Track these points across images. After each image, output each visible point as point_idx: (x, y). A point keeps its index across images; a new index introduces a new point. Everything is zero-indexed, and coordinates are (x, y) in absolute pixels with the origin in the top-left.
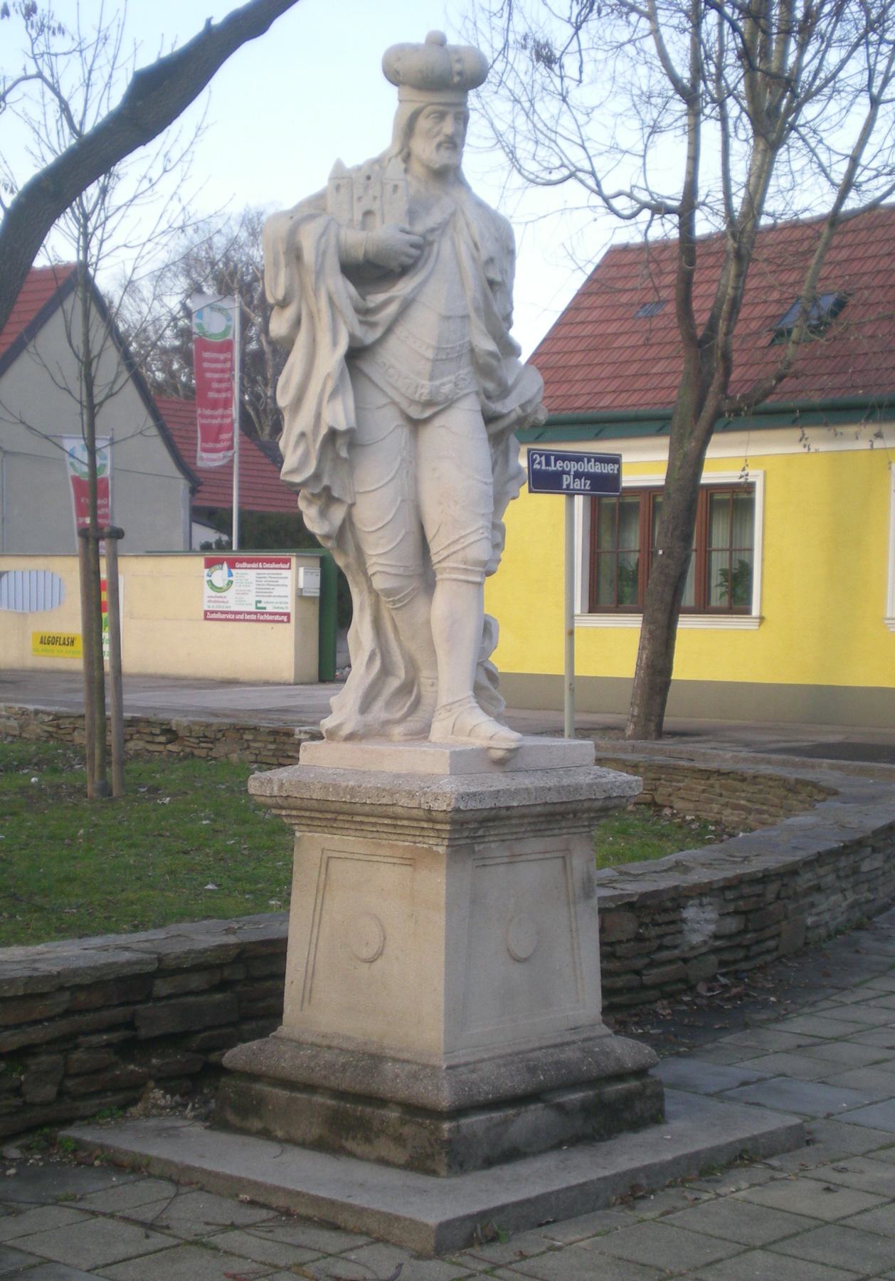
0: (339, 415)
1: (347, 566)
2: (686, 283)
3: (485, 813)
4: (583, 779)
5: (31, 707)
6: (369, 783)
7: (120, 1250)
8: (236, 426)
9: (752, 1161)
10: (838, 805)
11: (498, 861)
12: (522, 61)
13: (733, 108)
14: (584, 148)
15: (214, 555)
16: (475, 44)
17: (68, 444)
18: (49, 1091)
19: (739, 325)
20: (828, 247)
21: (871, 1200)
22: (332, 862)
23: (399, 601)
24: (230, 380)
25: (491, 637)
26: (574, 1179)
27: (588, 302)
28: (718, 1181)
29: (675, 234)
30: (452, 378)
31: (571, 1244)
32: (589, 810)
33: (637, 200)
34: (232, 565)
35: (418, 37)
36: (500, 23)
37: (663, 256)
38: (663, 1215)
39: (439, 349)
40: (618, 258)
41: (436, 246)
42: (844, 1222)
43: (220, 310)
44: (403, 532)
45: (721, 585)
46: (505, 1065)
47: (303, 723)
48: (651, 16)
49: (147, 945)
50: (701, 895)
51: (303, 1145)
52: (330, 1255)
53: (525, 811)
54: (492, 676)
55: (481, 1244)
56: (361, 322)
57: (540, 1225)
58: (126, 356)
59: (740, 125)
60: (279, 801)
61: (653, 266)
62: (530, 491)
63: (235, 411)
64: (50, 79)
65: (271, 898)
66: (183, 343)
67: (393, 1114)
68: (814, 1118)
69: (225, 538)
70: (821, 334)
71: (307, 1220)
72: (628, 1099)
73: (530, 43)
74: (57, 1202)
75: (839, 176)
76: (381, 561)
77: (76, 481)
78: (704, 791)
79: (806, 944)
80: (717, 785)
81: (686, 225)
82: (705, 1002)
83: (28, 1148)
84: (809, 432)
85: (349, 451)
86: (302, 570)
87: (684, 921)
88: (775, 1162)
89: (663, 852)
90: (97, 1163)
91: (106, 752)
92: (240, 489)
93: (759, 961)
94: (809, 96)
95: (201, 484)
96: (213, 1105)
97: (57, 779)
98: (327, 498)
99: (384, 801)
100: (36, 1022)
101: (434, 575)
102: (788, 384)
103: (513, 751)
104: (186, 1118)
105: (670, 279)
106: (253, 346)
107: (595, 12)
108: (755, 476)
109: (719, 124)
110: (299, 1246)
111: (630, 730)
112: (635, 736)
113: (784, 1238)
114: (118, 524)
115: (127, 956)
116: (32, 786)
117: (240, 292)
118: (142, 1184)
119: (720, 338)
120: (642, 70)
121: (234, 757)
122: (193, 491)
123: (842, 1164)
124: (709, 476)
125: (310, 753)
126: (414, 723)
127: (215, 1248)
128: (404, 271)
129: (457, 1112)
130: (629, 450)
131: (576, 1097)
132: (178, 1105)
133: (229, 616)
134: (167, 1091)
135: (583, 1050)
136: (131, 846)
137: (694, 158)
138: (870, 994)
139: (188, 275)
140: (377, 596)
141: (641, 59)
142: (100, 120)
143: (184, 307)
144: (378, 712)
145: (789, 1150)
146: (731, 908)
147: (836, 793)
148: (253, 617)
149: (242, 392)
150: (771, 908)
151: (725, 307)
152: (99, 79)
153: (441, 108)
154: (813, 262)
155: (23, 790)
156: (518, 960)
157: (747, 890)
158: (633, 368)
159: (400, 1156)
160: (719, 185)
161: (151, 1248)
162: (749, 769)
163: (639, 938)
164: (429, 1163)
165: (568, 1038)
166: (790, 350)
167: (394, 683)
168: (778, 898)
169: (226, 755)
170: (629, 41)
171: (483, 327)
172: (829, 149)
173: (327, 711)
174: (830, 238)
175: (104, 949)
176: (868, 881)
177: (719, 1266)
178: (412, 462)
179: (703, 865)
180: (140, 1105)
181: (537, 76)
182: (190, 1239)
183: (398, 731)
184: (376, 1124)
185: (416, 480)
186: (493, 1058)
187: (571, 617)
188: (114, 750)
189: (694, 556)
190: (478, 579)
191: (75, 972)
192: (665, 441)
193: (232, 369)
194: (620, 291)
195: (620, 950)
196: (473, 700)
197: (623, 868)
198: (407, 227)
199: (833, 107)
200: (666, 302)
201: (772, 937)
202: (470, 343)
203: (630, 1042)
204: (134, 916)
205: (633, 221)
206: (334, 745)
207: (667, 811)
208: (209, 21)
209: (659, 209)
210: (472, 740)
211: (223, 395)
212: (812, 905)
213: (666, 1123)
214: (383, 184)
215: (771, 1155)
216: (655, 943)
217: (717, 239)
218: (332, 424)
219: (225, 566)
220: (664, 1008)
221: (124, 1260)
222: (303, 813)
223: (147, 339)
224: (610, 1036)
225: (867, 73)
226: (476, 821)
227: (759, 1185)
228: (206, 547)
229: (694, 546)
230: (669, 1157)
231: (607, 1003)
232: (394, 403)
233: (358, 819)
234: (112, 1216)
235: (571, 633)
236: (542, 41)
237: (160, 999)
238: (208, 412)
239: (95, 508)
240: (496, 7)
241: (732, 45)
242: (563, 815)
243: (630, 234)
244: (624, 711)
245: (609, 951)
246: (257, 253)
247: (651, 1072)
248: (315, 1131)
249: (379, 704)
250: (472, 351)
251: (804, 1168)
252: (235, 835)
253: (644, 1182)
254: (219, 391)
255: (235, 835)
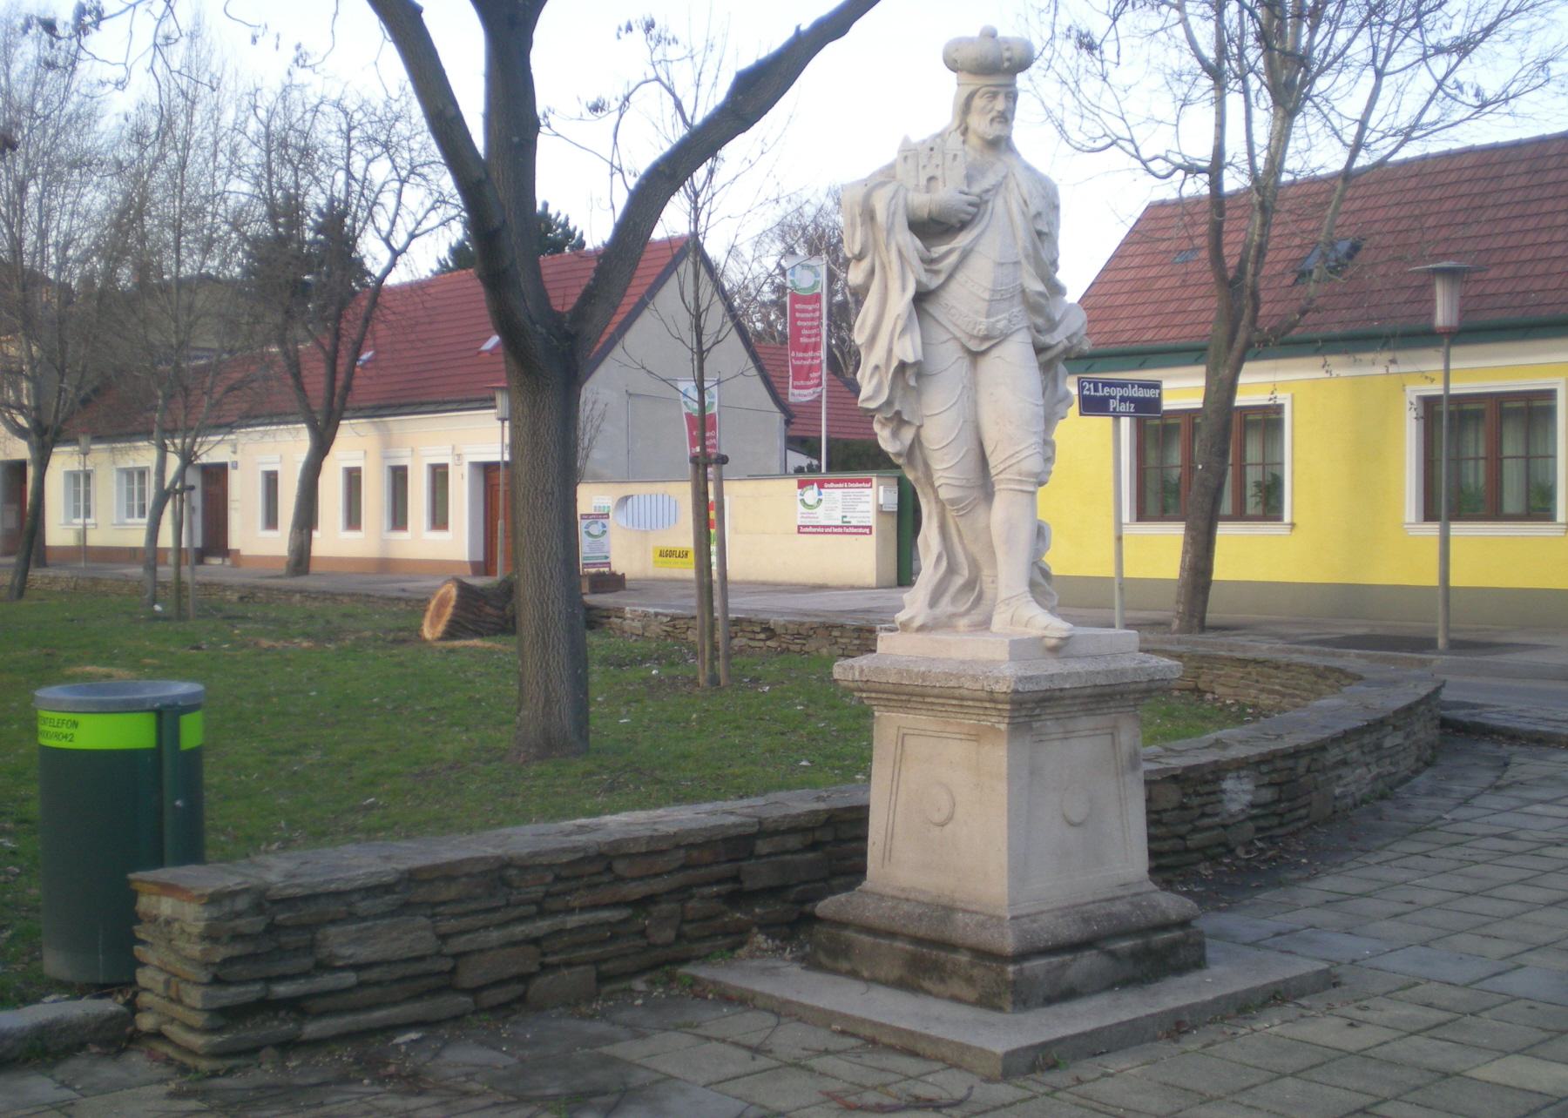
0: (908, 350)
1: (917, 480)
2: (1217, 232)
3: (1041, 695)
4: (1128, 664)
5: (652, 610)
6: (938, 668)
7: (731, 1070)
8: (824, 366)
9: (1284, 1000)
10: (1363, 688)
11: (1053, 736)
12: (1068, 48)
13: (1254, 83)
14: (1123, 119)
15: (805, 477)
16: (1027, 37)
17: (682, 386)
18: (669, 934)
19: (1266, 267)
20: (1342, 199)
21: (1390, 1034)
22: (906, 738)
23: (963, 509)
24: (819, 326)
25: (1044, 540)
26: (1125, 1016)
27: (1132, 249)
28: (1253, 1018)
29: (1206, 191)
30: (1006, 315)
31: (1122, 1071)
32: (1135, 692)
33: (1172, 163)
34: (821, 486)
35: (974, 32)
36: (1049, 18)
37: (1197, 209)
38: (1204, 1047)
39: (994, 291)
40: (1156, 214)
41: (990, 205)
42: (1365, 1053)
43: (809, 267)
44: (965, 449)
45: (1255, 495)
46: (1062, 917)
47: (884, 622)
48: (1180, 7)
49: (750, 810)
50: (1239, 768)
51: (886, 983)
52: (910, 1078)
53: (1077, 692)
54: (1045, 573)
55: (1042, 1070)
56: (926, 271)
57: (1095, 1055)
58: (730, 308)
59: (1261, 96)
60: (860, 684)
61: (1187, 219)
62: (1081, 414)
63: (823, 354)
64: (666, 81)
65: (857, 773)
66: (779, 298)
67: (964, 958)
68: (1339, 964)
69: (815, 462)
70: (1339, 274)
71: (891, 1048)
72: (1173, 946)
73: (1074, 34)
74: (677, 1028)
75: (1349, 138)
76: (945, 474)
77: (689, 416)
78: (1242, 678)
79: (1335, 812)
80: (1254, 674)
81: (1216, 183)
82: (1243, 863)
83: (652, 983)
84: (1332, 359)
85: (917, 381)
86: (881, 488)
87: (1223, 791)
88: (1304, 1002)
89: (1205, 731)
90: (710, 996)
91: (714, 648)
92: (828, 420)
93: (1290, 828)
94: (1320, 72)
95: (795, 417)
96: (808, 948)
97: (675, 671)
98: (898, 421)
99: (952, 684)
100: (657, 875)
101: (993, 486)
102: (1311, 317)
103: (1065, 640)
104: (784, 960)
105: (1204, 228)
106: (839, 298)
107: (1130, 5)
108: (1283, 398)
109: (1242, 97)
110: (883, 1070)
111: (1175, 625)
112: (1180, 631)
113: (1312, 1067)
114: (724, 452)
115: (732, 819)
116: (653, 677)
117: (828, 253)
118: (749, 1015)
119: (1249, 278)
120: (1174, 53)
121: (824, 651)
122: (788, 423)
123: (1364, 1003)
124: (1242, 399)
125: (886, 643)
126: (976, 616)
127: (811, 1070)
128: (963, 226)
129: (1021, 956)
130: (1168, 377)
131: (1125, 944)
132: (778, 948)
133: (819, 530)
134: (768, 936)
135: (1132, 904)
136: (738, 728)
137: (1220, 126)
138: (1390, 855)
139: (783, 239)
140: (943, 505)
141: (1172, 43)
142: (707, 113)
143: (779, 265)
144: (945, 606)
145: (1317, 992)
146: (1266, 780)
147: (1361, 678)
148: (840, 530)
149: (829, 337)
150: (1302, 780)
151: (1252, 252)
152: (707, 80)
153: (993, 89)
154: (1329, 211)
155: (646, 680)
156: (1072, 824)
157: (1279, 764)
158: (1172, 307)
159: (972, 994)
160: (1244, 147)
161: (757, 1069)
162: (1283, 658)
163: (1183, 807)
164: (996, 1000)
165: (1119, 893)
166: (1312, 289)
167: (959, 581)
168: (1308, 770)
169: (817, 650)
170: (1162, 29)
171: (1031, 270)
172: (1340, 115)
173: (901, 608)
174: (1344, 190)
175: (713, 813)
176: (1390, 756)
177: (1253, 1091)
178: (972, 387)
179: (1240, 742)
180: (746, 948)
181: (1081, 61)
182: (790, 1061)
183: (963, 623)
184: (949, 966)
185: (975, 404)
186: (1053, 910)
187: (1119, 524)
188: (721, 645)
189: (1230, 471)
190: (1032, 489)
191: (689, 832)
192: (1202, 369)
193: (820, 318)
194: (1158, 240)
195: (1166, 817)
196: (1029, 595)
197: (1168, 745)
198: (965, 189)
199: (1343, 79)
200: (1199, 249)
201: (1304, 806)
202: (1021, 285)
203: (1174, 896)
204: (739, 788)
205: (1168, 180)
206: (906, 635)
207: (1209, 696)
208: (798, 28)
209: (1191, 169)
210: (1029, 630)
211: (813, 340)
212: (1340, 777)
213: (1208, 968)
214: (944, 155)
215: (1302, 995)
216: (1197, 812)
217: (1245, 194)
218: (902, 357)
219: (815, 486)
220: (1206, 869)
221: (734, 1078)
222: (880, 695)
223: (749, 295)
224: (1155, 891)
225: (1371, 50)
226: (1033, 701)
227: (1291, 1021)
228: (799, 470)
229: (1230, 461)
230: (1209, 997)
231: (1154, 864)
232: (955, 338)
233: (929, 700)
234: (724, 1041)
235: (1119, 539)
236: (1084, 32)
237: (760, 857)
238: (800, 355)
239: (704, 439)
240: (1044, 5)
241: (1252, 29)
242: (1111, 696)
243: (1167, 191)
244: (1170, 608)
245: (1155, 817)
246: (840, 219)
247: (1194, 923)
248: (896, 973)
249: (946, 599)
250: (1023, 291)
251: (1330, 1007)
252: (826, 718)
253: (1187, 1018)
254: (809, 336)
255: (826, 718)
